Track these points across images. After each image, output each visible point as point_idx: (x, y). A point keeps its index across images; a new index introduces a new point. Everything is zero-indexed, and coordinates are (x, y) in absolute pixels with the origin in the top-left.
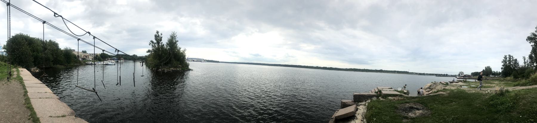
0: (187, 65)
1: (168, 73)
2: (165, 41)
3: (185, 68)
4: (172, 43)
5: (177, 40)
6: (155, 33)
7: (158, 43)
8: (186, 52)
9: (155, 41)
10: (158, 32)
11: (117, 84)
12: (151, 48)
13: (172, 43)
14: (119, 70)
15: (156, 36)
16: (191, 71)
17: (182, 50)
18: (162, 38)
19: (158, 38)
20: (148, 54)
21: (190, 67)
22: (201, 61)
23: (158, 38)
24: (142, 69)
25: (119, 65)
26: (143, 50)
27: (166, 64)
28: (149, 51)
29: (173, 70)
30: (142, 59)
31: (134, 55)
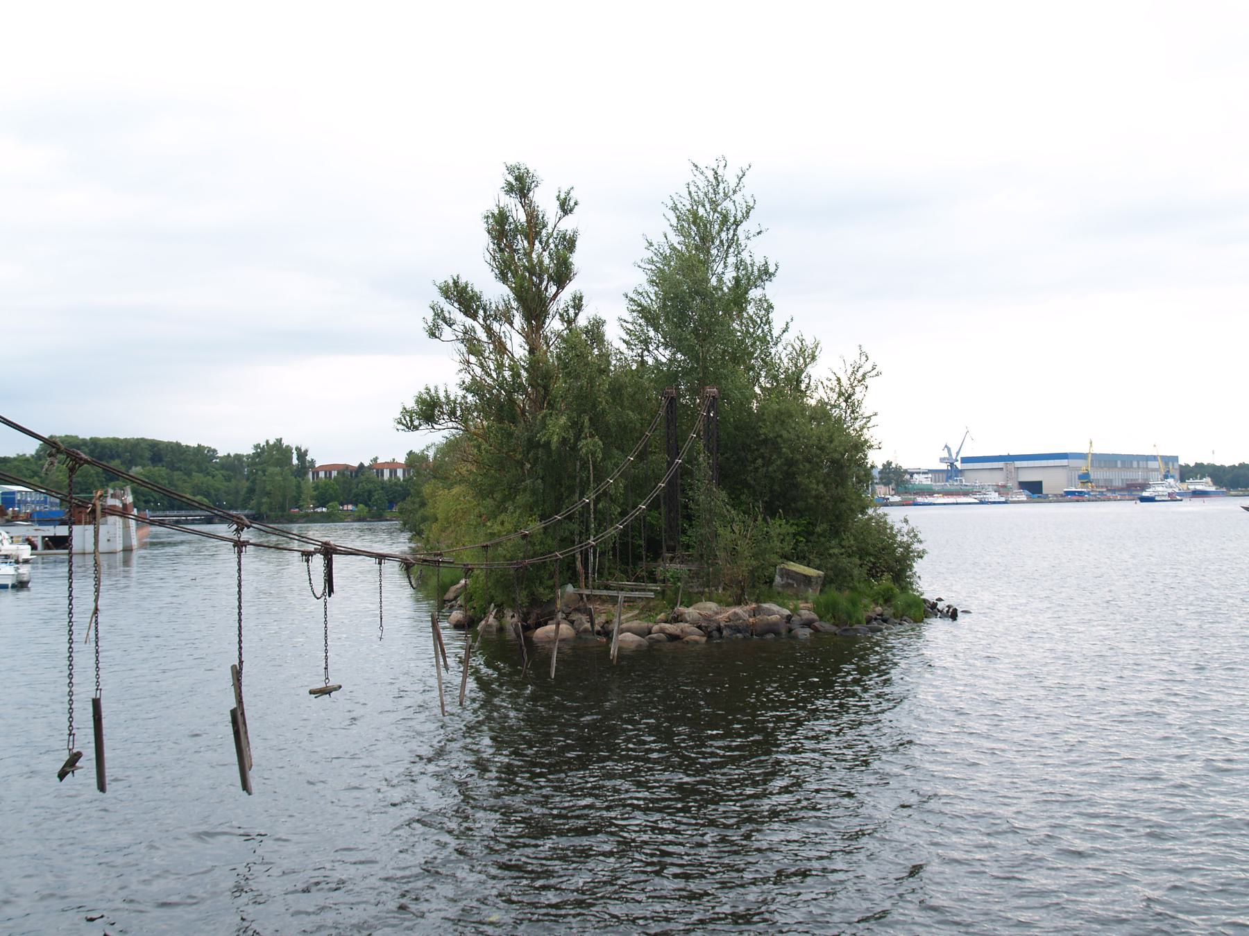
0: (891, 563)
1: (651, 659)
2: (609, 292)
3: (873, 592)
4: (702, 299)
5: (756, 251)
6: (493, 195)
7: (534, 308)
8: (870, 400)
9: (495, 292)
10: (521, 186)
11: (73, 761)
12: (446, 371)
13: (702, 299)
14: (83, 633)
15: (500, 227)
16: (936, 629)
17: (821, 383)
18: (569, 243)
19: (530, 254)
20: (429, 440)
21: (929, 581)
22: (1135, 491)
23: (530, 254)
24: (366, 646)
25: (84, 587)
26: (366, 394)
27: (637, 554)
28: (428, 410)
29: (710, 630)
30: (363, 494)
31: (274, 456)
